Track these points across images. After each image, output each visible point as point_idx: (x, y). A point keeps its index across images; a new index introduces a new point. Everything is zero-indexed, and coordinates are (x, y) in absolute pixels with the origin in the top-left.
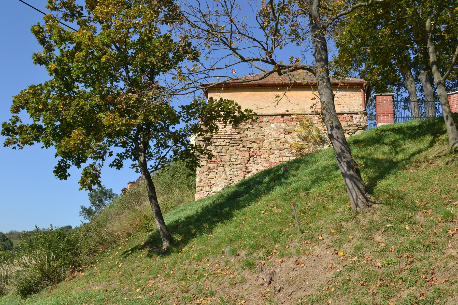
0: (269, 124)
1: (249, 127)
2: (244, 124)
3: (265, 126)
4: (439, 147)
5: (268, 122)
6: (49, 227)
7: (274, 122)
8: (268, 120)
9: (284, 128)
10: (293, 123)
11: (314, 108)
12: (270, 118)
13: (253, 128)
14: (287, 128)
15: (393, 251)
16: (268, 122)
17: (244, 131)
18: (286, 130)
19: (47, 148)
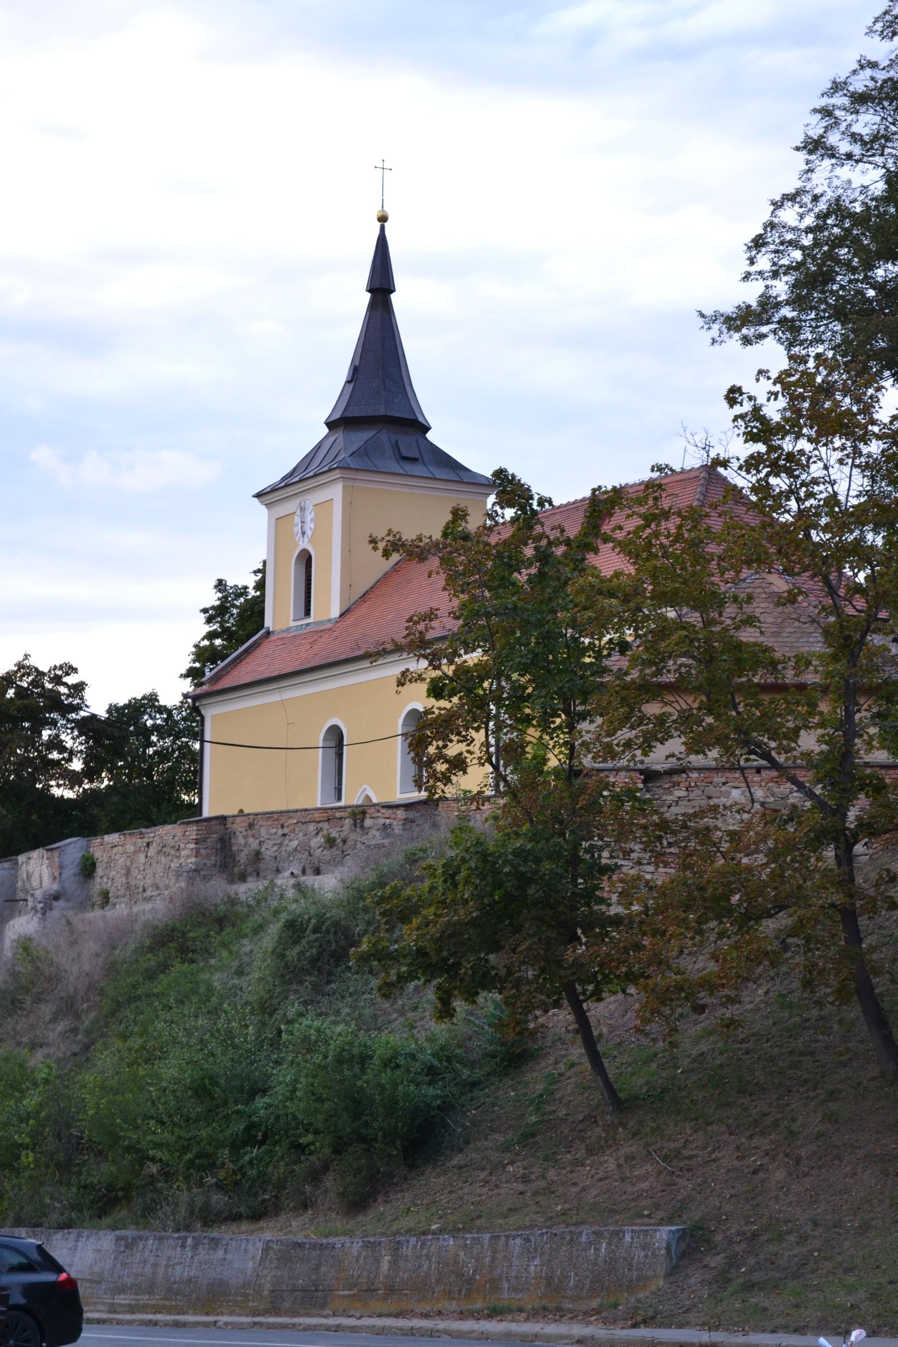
0: (726, 791)
1: (680, 798)
2: (667, 786)
3: (718, 795)
4: (510, 1038)
5: (724, 784)
6: (250, 581)
7: (738, 785)
8: (724, 780)
9: (762, 800)
10: (782, 787)
11: (420, 1010)
12: (729, 775)
13: (689, 801)
14: (768, 800)
15: (220, 1115)
16: (724, 784)
17: (669, 807)
18: (767, 806)
19: (220, 585)
